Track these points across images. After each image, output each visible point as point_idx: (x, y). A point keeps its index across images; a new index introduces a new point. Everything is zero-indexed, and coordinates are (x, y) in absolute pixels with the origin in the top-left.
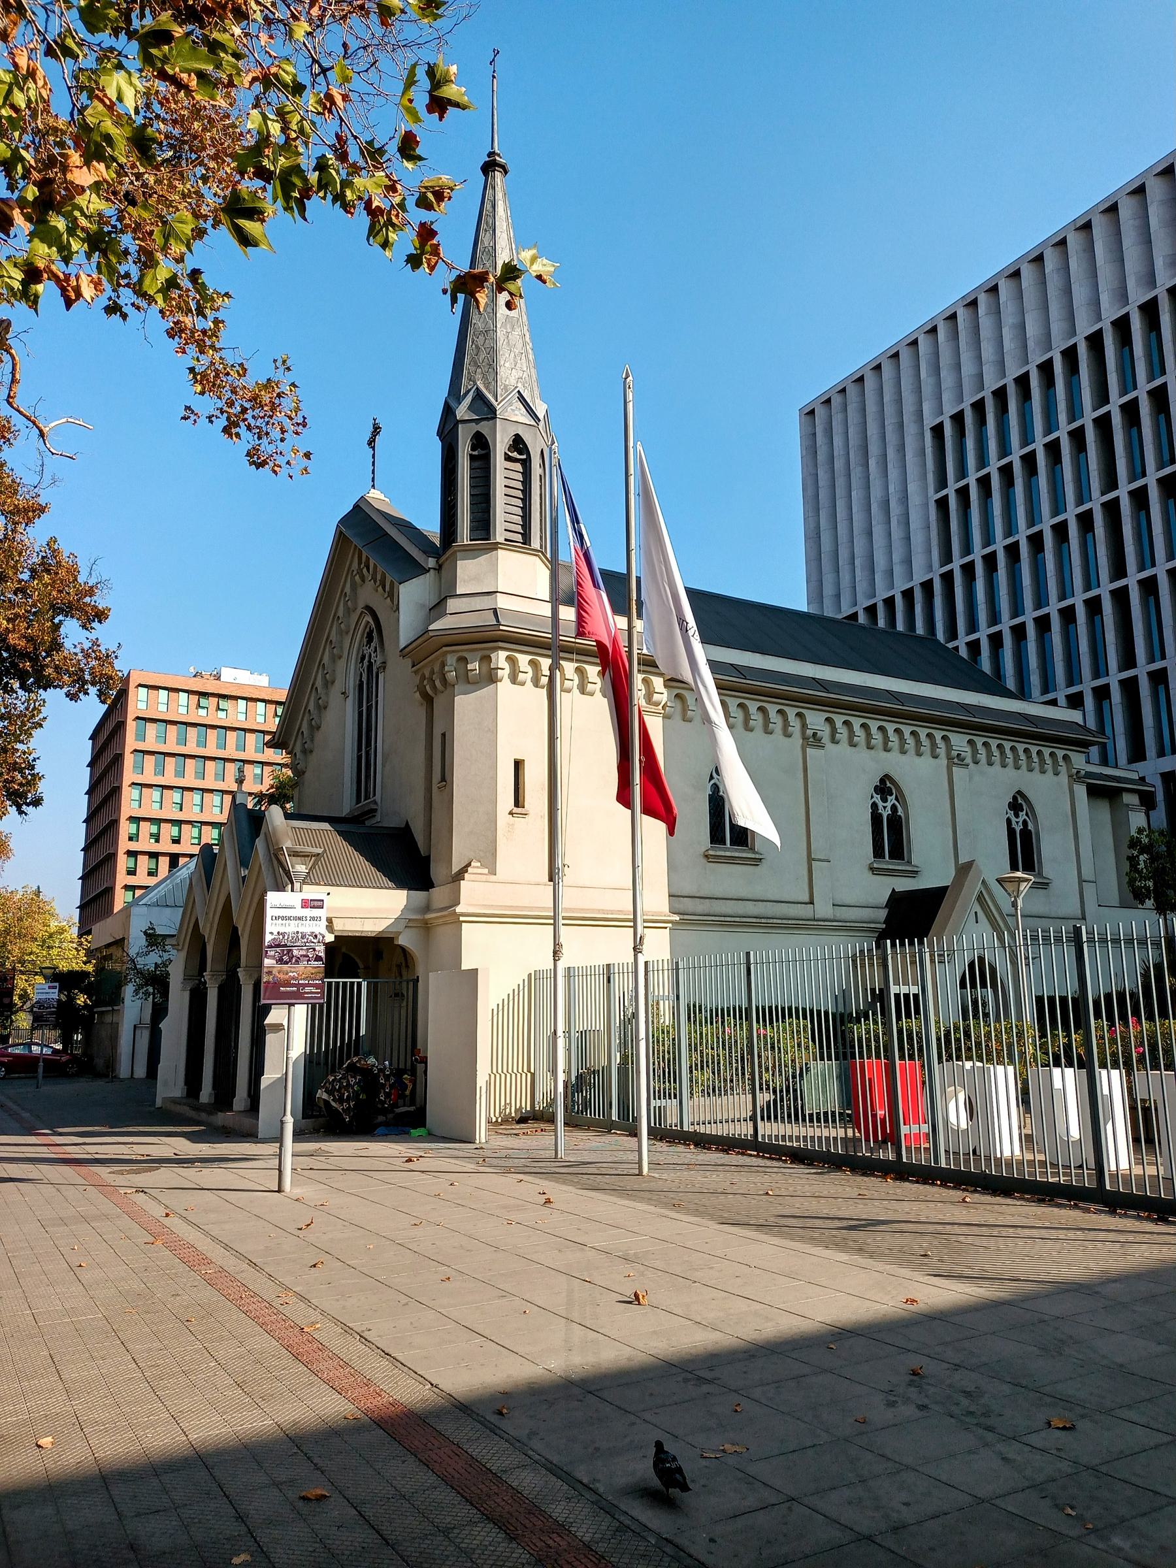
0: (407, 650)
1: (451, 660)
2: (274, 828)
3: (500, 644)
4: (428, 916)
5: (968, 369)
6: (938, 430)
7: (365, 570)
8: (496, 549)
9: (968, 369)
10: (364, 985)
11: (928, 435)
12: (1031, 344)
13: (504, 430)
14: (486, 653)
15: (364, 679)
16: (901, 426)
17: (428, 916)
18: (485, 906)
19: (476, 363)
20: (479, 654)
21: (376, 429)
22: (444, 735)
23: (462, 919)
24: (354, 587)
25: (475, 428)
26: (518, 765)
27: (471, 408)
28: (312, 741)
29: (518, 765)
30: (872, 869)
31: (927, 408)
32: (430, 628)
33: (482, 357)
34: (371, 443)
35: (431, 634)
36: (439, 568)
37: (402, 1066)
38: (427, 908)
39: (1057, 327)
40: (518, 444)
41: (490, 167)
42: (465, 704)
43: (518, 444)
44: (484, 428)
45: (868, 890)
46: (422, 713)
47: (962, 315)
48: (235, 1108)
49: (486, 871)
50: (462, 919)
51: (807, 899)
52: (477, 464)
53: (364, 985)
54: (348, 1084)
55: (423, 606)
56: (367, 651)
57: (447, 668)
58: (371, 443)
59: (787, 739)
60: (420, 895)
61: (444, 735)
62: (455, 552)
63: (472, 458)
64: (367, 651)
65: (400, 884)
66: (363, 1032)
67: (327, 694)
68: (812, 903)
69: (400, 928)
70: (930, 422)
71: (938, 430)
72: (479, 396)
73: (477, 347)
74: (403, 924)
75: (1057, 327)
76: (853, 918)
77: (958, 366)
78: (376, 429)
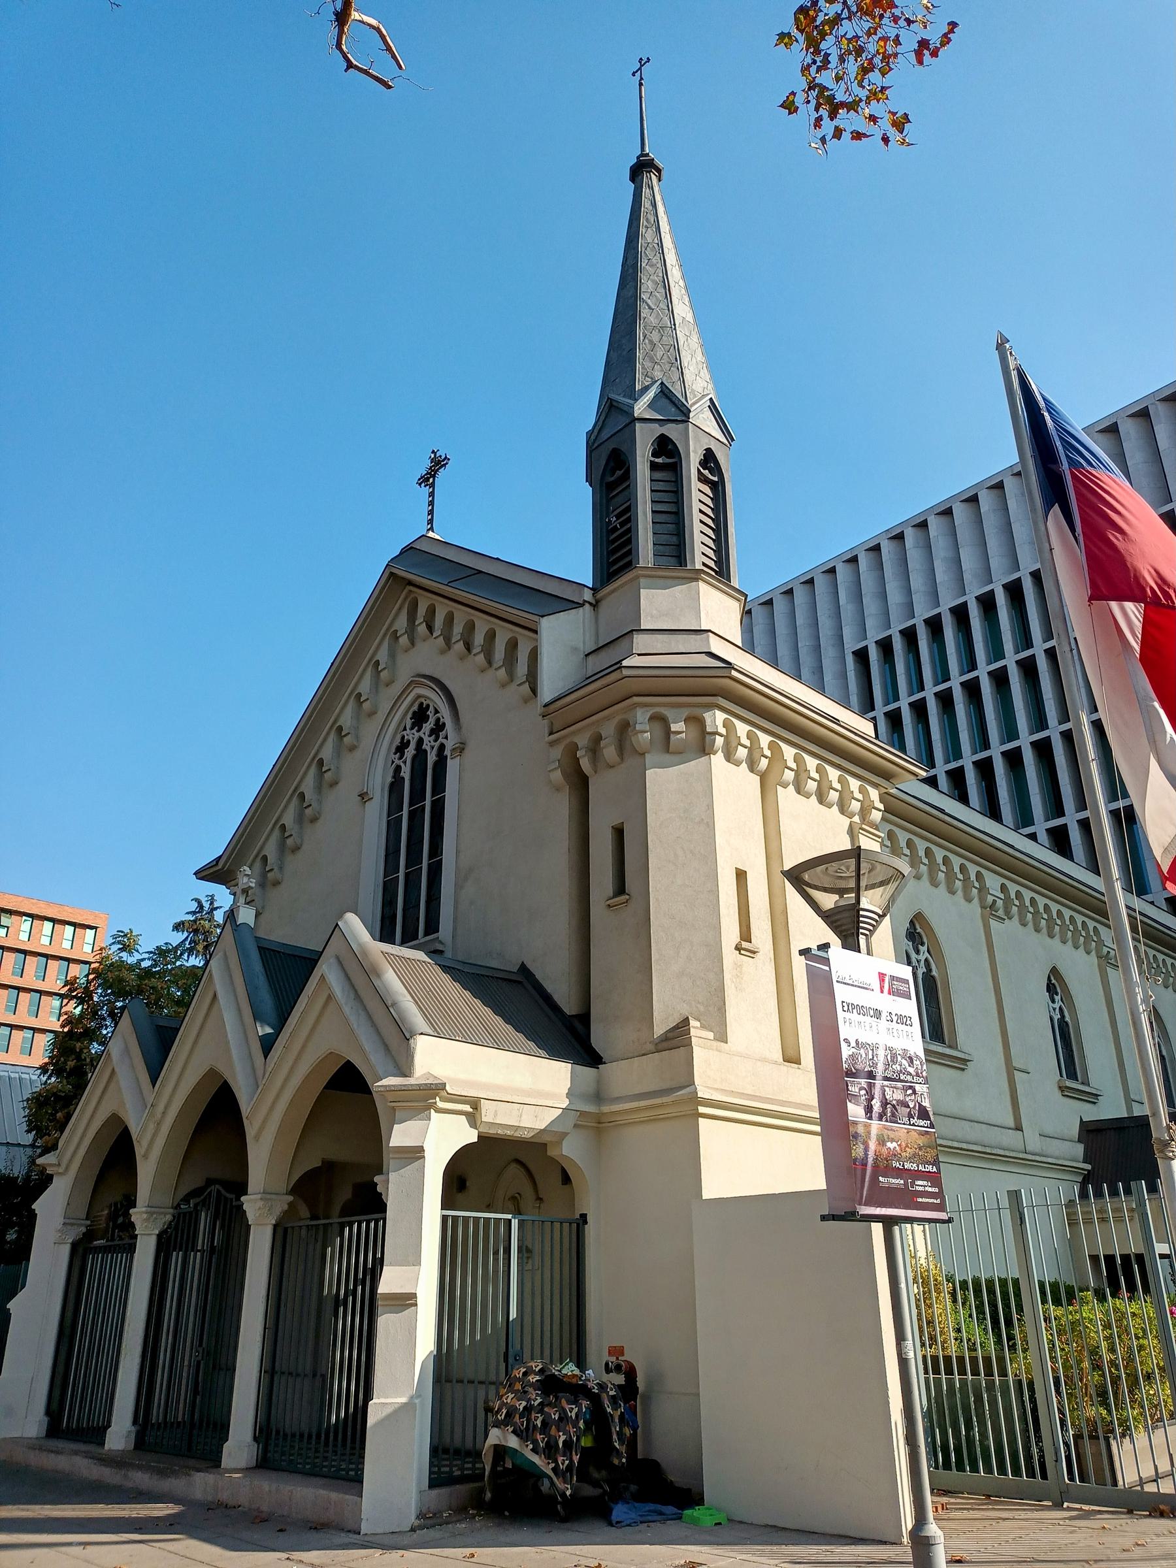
0: (552, 707)
1: (641, 717)
2: (360, 945)
3: (721, 701)
4: (606, 1109)
5: (895, 596)
6: (862, 656)
7: (422, 629)
8: (697, 580)
9: (895, 596)
10: (515, 1223)
11: (850, 660)
12: (967, 577)
13: (697, 439)
14: (696, 711)
15: (406, 773)
16: (817, 648)
17: (606, 1109)
18: (723, 1091)
19: (652, 359)
20: (685, 712)
21: (438, 463)
22: (619, 832)
23: (702, 1110)
24: (392, 655)
25: (658, 430)
26: (741, 875)
27: (652, 405)
28: (281, 868)
29: (741, 875)
30: (1062, 1089)
31: (848, 633)
32: (625, 663)
33: (659, 354)
34: (428, 479)
35: (625, 672)
36: (595, 605)
37: (291, 1380)
38: (598, 1097)
39: (997, 562)
40: (709, 459)
41: (642, 168)
42: (663, 783)
43: (709, 459)
44: (672, 431)
45: (1056, 1121)
46: (562, 806)
47: (886, 547)
48: (226, 1462)
49: (711, 1035)
50: (702, 1110)
51: (1012, 1124)
52: (658, 475)
53: (515, 1223)
54: (564, 1418)
55: (575, 649)
56: (412, 736)
57: (603, 743)
58: (428, 479)
59: (966, 904)
60: (587, 1072)
61: (619, 832)
62: (637, 577)
63: (654, 467)
64: (412, 736)
65: (555, 1053)
66: (513, 1314)
67: (320, 802)
68: (1019, 1128)
69: (567, 1126)
70: (851, 645)
71: (862, 656)
72: (665, 393)
73: (651, 342)
74: (572, 1118)
75: (997, 562)
76: (1057, 1153)
77: (883, 596)
78: (438, 463)
